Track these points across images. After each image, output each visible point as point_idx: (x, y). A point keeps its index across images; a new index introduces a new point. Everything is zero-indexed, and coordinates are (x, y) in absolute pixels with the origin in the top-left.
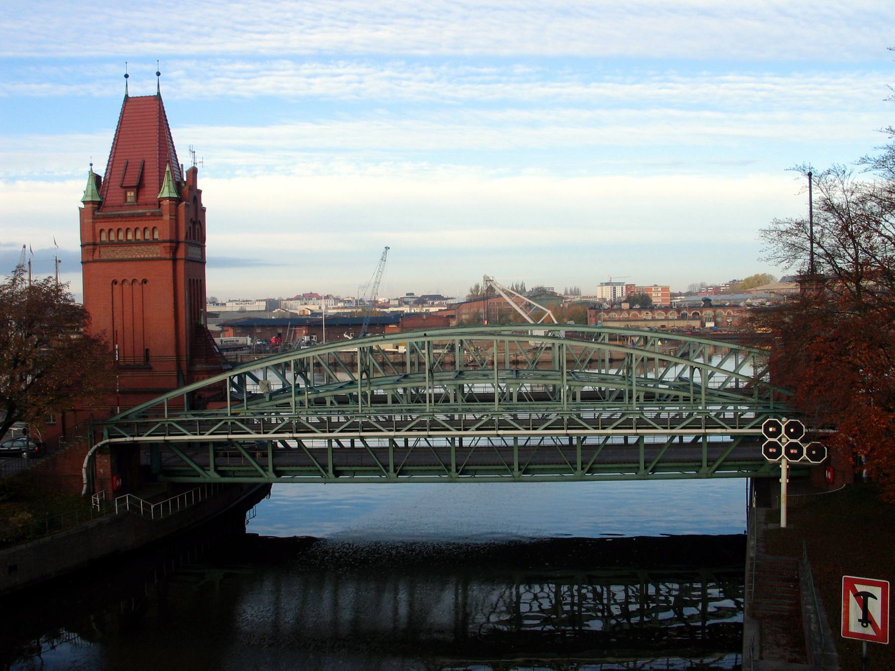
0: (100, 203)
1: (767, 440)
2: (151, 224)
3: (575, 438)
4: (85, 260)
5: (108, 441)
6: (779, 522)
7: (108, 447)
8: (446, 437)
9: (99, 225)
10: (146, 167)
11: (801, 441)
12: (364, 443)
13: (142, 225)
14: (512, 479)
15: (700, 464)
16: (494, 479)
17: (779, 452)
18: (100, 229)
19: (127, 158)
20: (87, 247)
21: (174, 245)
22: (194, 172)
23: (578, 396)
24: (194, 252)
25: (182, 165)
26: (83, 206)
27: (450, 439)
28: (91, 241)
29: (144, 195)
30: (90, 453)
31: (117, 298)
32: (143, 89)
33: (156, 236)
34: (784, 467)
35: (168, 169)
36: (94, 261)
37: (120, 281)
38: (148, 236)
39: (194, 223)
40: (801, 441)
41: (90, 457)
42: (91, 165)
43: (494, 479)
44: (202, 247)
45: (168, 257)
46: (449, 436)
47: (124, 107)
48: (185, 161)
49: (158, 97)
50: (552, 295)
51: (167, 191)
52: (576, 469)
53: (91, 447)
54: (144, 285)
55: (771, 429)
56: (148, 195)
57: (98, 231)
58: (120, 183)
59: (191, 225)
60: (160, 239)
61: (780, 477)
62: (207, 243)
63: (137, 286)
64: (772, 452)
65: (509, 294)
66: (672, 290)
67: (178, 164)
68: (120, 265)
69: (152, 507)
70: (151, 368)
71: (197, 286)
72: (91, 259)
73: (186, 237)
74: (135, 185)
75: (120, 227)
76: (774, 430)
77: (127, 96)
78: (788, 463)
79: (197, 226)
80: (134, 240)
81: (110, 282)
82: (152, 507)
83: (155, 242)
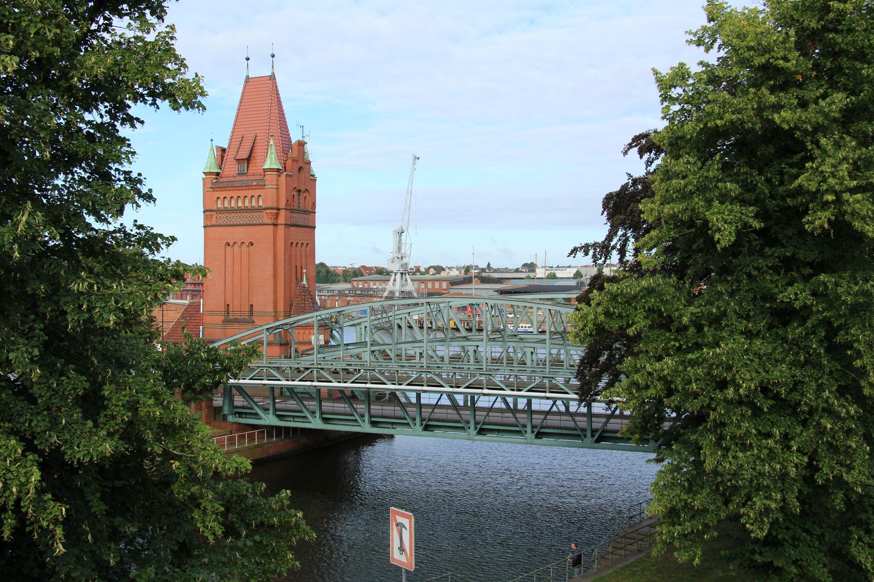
0: (218, 174)
2: (256, 193)
3: (559, 402)
10: (257, 141)
13: (249, 193)
19: (243, 133)
21: (275, 211)
26: (204, 176)
28: (274, 205)
31: (229, 257)
32: (259, 70)
33: (261, 204)
36: (212, 226)
38: (247, 204)
49: (272, 78)
50: (326, 266)
52: (585, 436)
58: (234, 156)
60: (264, 207)
63: (244, 247)
73: (286, 204)
74: (245, 158)
75: (232, 195)
77: (248, 77)
80: (250, 207)
83: (260, 209)
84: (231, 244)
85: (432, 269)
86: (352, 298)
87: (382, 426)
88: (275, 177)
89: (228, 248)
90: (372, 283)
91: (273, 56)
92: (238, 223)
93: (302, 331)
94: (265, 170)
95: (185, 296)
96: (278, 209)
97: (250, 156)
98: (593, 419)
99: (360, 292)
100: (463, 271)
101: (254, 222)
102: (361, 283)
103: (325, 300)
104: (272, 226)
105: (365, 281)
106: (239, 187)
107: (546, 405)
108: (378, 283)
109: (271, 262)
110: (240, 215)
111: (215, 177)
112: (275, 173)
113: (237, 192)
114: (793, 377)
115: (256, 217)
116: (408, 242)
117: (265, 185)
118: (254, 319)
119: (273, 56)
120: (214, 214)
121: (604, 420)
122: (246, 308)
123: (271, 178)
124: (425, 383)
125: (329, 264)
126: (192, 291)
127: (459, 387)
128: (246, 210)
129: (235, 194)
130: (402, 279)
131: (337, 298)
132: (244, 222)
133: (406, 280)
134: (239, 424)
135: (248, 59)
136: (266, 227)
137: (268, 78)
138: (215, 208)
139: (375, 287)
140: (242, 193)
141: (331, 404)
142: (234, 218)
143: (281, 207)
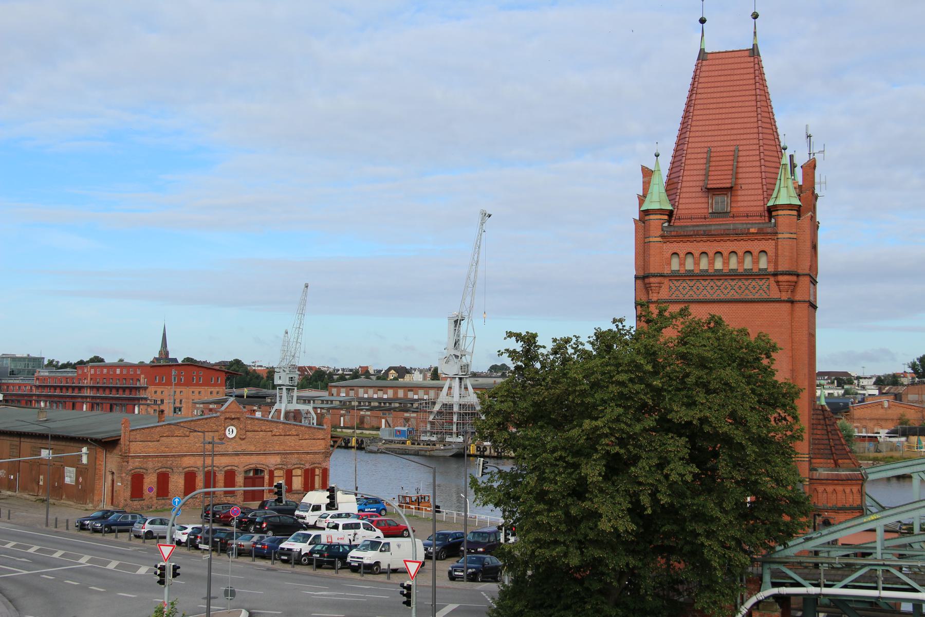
0: (670, 214)
2: (755, 246)
7: (771, 600)
18: (670, 252)
21: (794, 278)
22: (810, 167)
49: (754, 52)
80: (741, 270)
85: (393, 371)
86: (368, 413)
90: (361, 391)
91: (755, 16)
92: (715, 297)
95: (77, 405)
96: (798, 275)
99: (376, 404)
100: (429, 375)
101: (751, 297)
102: (343, 390)
103: (322, 414)
104: (789, 305)
105: (352, 388)
108: (371, 391)
110: (719, 283)
113: (716, 244)
114: (419, 509)
116: (470, 333)
117: (776, 233)
119: (755, 16)
120: (666, 281)
125: (246, 361)
126: (93, 397)
128: (733, 275)
129: (711, 248)
130: (460, 387)
131: (343, 412)
132: (729, 297)
133: (466, 388)
136: (777, 305)
138: (666, 271)
139: (366, 396)
143: (800, 272)
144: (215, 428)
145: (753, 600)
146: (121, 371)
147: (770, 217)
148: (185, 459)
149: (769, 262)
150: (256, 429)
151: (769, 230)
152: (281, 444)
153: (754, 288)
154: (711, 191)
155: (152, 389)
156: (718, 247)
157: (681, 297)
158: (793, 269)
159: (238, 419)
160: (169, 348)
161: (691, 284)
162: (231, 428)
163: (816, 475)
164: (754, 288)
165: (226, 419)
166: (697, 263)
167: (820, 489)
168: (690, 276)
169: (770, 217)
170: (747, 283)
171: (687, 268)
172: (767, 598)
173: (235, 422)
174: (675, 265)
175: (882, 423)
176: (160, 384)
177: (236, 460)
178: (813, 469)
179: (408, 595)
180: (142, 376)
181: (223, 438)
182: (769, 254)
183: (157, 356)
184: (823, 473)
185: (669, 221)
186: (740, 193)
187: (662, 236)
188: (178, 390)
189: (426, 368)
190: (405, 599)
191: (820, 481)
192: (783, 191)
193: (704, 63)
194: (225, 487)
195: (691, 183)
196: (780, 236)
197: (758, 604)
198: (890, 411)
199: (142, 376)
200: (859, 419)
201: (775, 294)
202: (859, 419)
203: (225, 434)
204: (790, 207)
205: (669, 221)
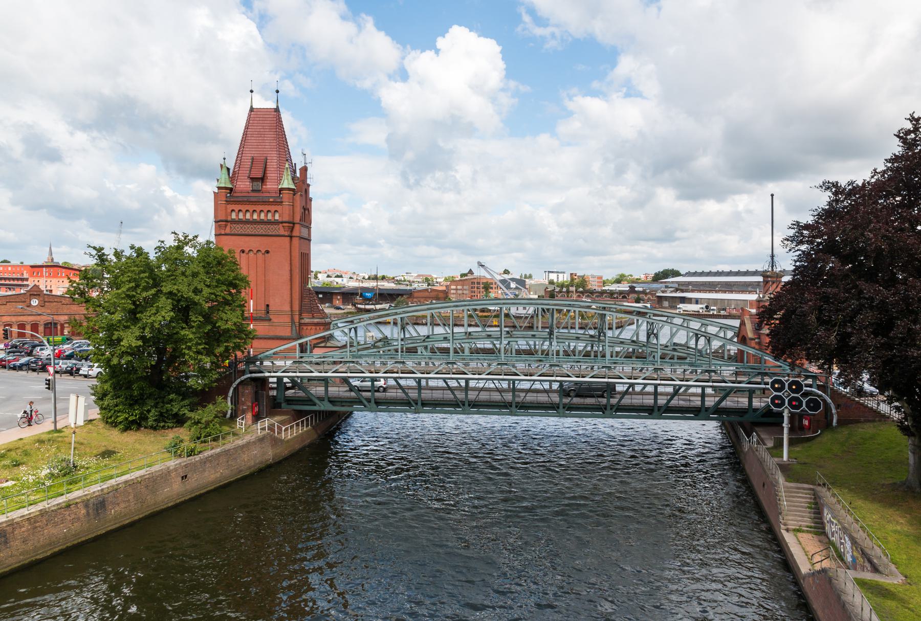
0: (231, 189)
1: (801, 395)
2: (273, 208)
4: (218, 233)
5: (249, 375)
6: (783, 457)
7: (249, 380)
8: (414, 378)
9: (230, 207)
11: (801, 395)
12: (446, 383)
13: (266, 208)
14: (557, 414)
15: (797, 417)
16: (540, 414)
17: (783, 404)
18: (231, 209)
20: (220, 223)
21: (292, 225)
22: (304, 170)
23: (514, 351)
24: (304, 232)
25: (295, 164)
27: (417, 380)
29: (266, 185)
30: (234, 385)
32: (264, 103)
34: (786, 415)
35: (287, 166)
37: (247, 251)
38: (255, 216)
39: (305, 209)
40: (801, 395)
41: (235, 389)
42: (224, 159)
43: (540, 414)
44: (309, 228)
45: (286, 235)
46: (417, 378)
47: (249, 115)
48: (298, 160)
49: (277, 110)
51: (287, 183)
53: (235, 381)
54: (266, 254)
55: (776, 386)
56: (270, 185)
57: (229, 211)
58: (247, 175)
59: (303, 211)
60: (280, 220)
61: (783, 423)
62: (312, 225)
64: (778, 403)
65: (66, 294)
66: (604, 278)
67: (292, 164)
68: (247, 238)
69: (283, 429)
70: (270, 320)
71: (305, 258)
72: (223, 233)
76: (780, 386)
78: (790, 412)
79: (307, 212)
81: (239, 251)
82: (283, 429)
83: (276, 223)
84: (247, 251)
87: (294, 403)
88: (292, 195)
89: (242, 254)
91: (277, 92)
93: (313, 327)
94: (281, 190)
96: (294, 224)
97: (264, 176)
98: (516, 393)
101: (270, 233)
104: (289, 238)
106: (255, 202)
107: (526, 385)
109: (287, 268)
110: (255, 226)
111: (229, 191)
112: (292, 192)
115: (272, 229)
117: (282, 202)
118: (271, 317)
121: (477, 393)
122: (264, 308)
123: (286, 196)
124: (400, 372)
127: (327, 372)
129: (251, 208)
132: (260, 233)
134: (295, 410)
135: (252, 91)
136: (283, 238)
137: (273, 110)
138: (229, 219)
140: (258, 208)
141: (634, 401)
142: (249, 229)
143: (295, 222)
144: (23, 300)
145: (239, 380)
146: (12, 269)
147: (280, 194)
148: (5, 317)
149: (279, 216)
150: (51, 300)
151: (279, 200)
152: (68, 309)
153: (272, 229)
154: (253, 179)
155: (31, 279)
156: (255, 208)
157: (236, 232)
158: (291, 220)
159: (39, 295)
160: (54, 256)
161: (242, 226)
162: (35, 300)
163: (303, 321)
164: (272, 229)
165: (30, 295)
166: (245, 216)
167: (305, 328)
168: (240, 222)
169: (280, 194)
170: (269, 226)
171: (276, 218)
172: (246, 379)
173: (37, 297)
174: (234, 216)
175: (428, 299)
176: (37, 276)
177: (38, 318)
178: (300, 319)
179: (49, 384)
180: (25, 272)
181: (29, 306)
182: (279, 212)
183: (47, 261)
184: (307, 321)
185: (230, 193)
186: (268, 181)
187: (226, 201)
188: (49, 280)
189: (610, 279)
190: (47, 386)
191: (306, 324)
192: (286, 181)
193: (252, 113)
194: (31, 331)
195: (244, 172)
196: (284, 203)
197: (242, 382)
198: (431, 294)
199: (25, 272)
200: (417, 298)
201: (282, 232)
202: (417, 298)
203: (30, 303)
204: (289, 189)
205: (230, 193)
